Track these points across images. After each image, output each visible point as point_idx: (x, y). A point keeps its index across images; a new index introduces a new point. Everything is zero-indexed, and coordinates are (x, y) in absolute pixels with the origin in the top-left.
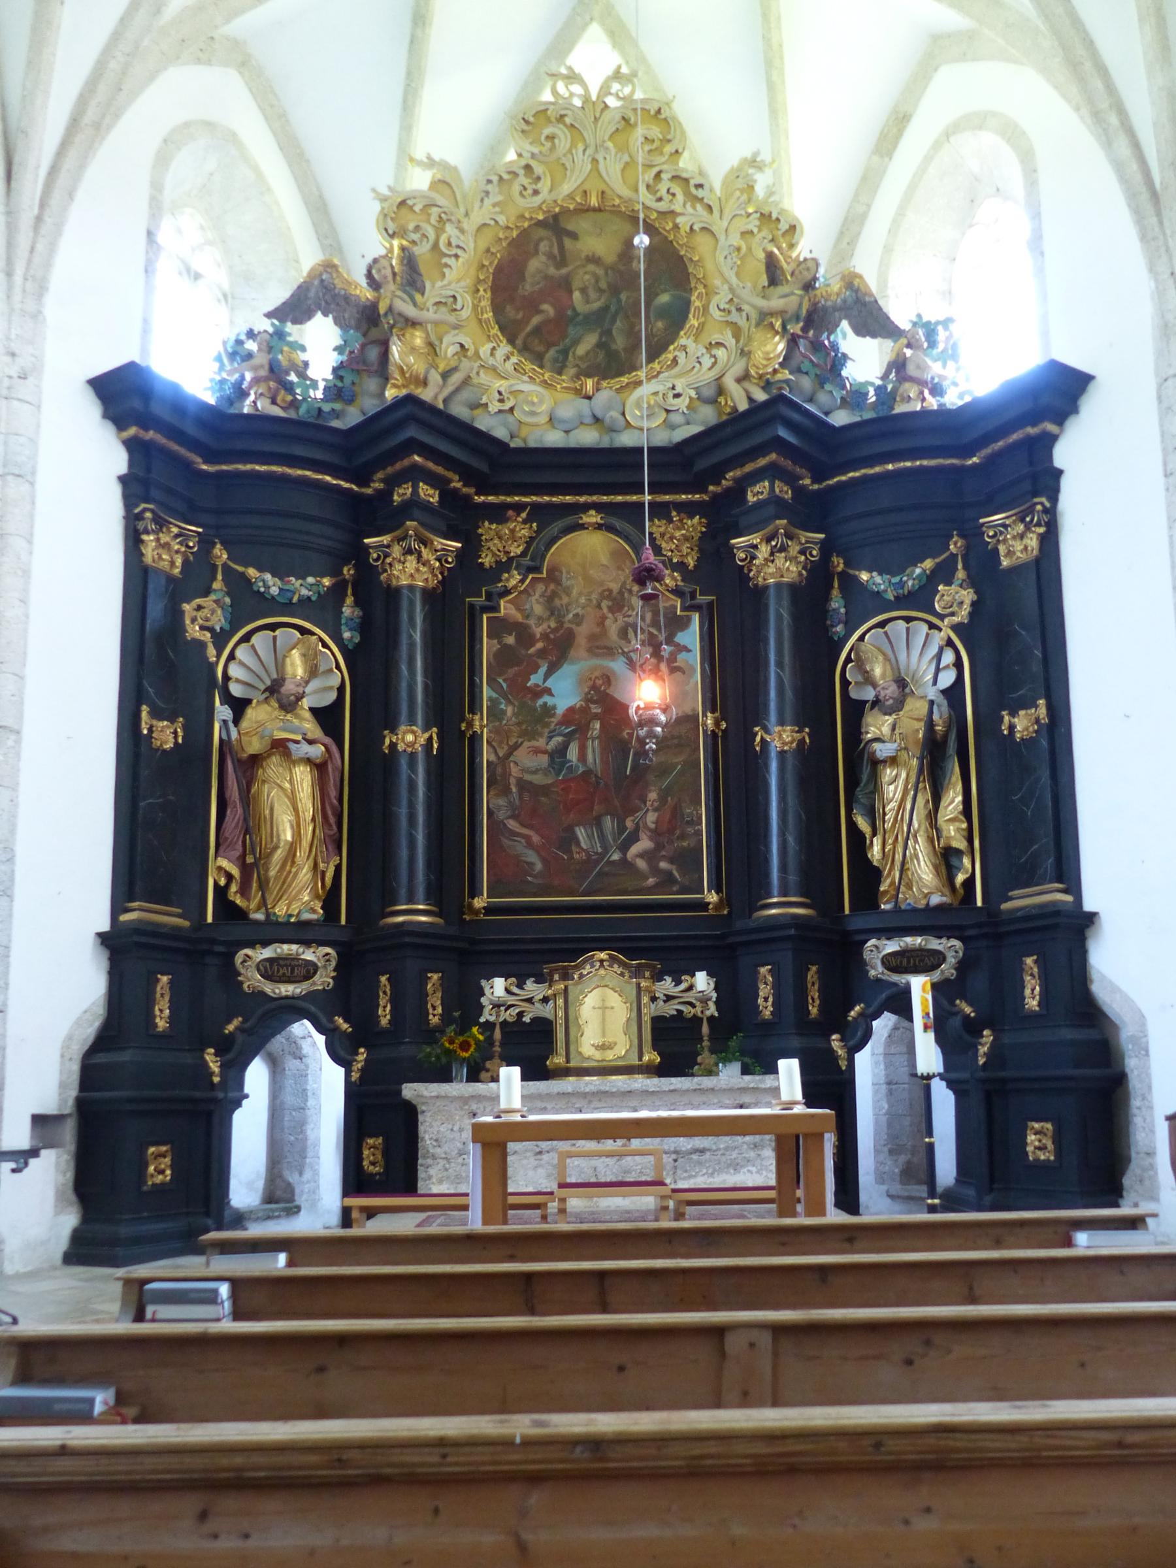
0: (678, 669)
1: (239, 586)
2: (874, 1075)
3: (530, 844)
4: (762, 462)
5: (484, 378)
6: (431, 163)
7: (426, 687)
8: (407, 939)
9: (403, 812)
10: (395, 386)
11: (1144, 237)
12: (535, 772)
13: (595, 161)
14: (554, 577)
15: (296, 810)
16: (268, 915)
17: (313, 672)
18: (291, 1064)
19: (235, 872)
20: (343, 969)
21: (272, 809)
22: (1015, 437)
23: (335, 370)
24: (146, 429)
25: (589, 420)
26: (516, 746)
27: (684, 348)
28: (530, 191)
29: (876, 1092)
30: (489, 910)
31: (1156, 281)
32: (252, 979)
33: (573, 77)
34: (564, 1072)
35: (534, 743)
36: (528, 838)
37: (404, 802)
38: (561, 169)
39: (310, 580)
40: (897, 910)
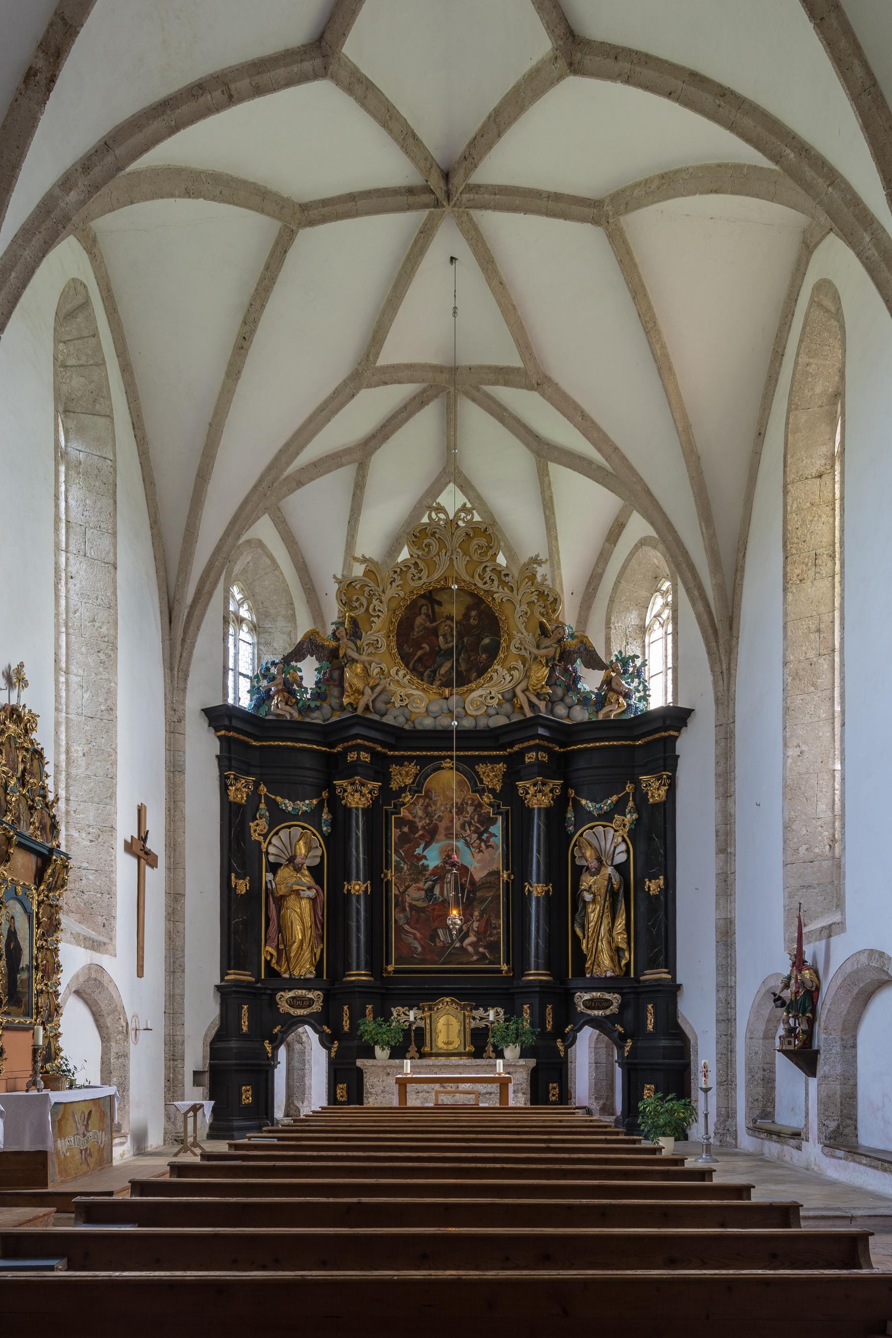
0: (491, 846)
1: (273, 806)
2: (590, 1059)
3: (415, 938)
4: (532, 743)
5: (393, 687)
6: (364, 560)
7: (364, 859)
8: (357, 989)
9: (354, 924)
10: (348, 696)
11: (709, 653)
12: (418, 900)
13: (451, 559)
14: (428, 796)
15: (303, 923)
16: (291, 975)
17: (309, 849)
18: (297, 1047)
19: (275, 953)
20: (326, 1001)
21: (292, 923)
22: (657, 736)
23: (317, 683)
24: (230, 731)
25: (446, 711)
26: (408, 887)
27: (496, 671)
28: (416, 577)
29: (590, 1068)
30: (395, 972)
31: (714, 676)
32: (284, 1007)
33: (440, 509)
34: (431, 1055)
35: (418, 885)
36: (414, 934)
37: (355, 919)
38: (432, 565)
39: (307, 802)
40: (592, 977)
